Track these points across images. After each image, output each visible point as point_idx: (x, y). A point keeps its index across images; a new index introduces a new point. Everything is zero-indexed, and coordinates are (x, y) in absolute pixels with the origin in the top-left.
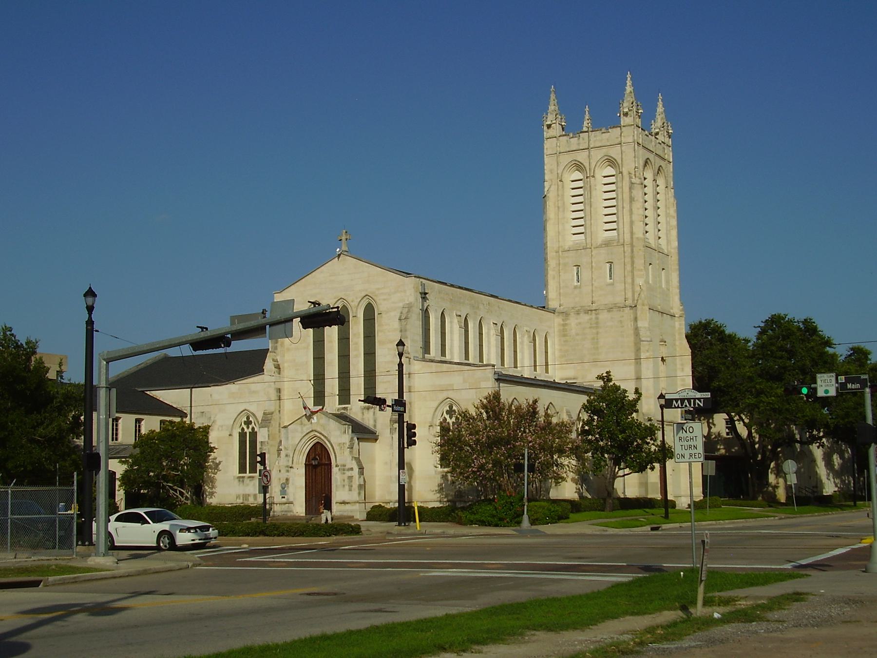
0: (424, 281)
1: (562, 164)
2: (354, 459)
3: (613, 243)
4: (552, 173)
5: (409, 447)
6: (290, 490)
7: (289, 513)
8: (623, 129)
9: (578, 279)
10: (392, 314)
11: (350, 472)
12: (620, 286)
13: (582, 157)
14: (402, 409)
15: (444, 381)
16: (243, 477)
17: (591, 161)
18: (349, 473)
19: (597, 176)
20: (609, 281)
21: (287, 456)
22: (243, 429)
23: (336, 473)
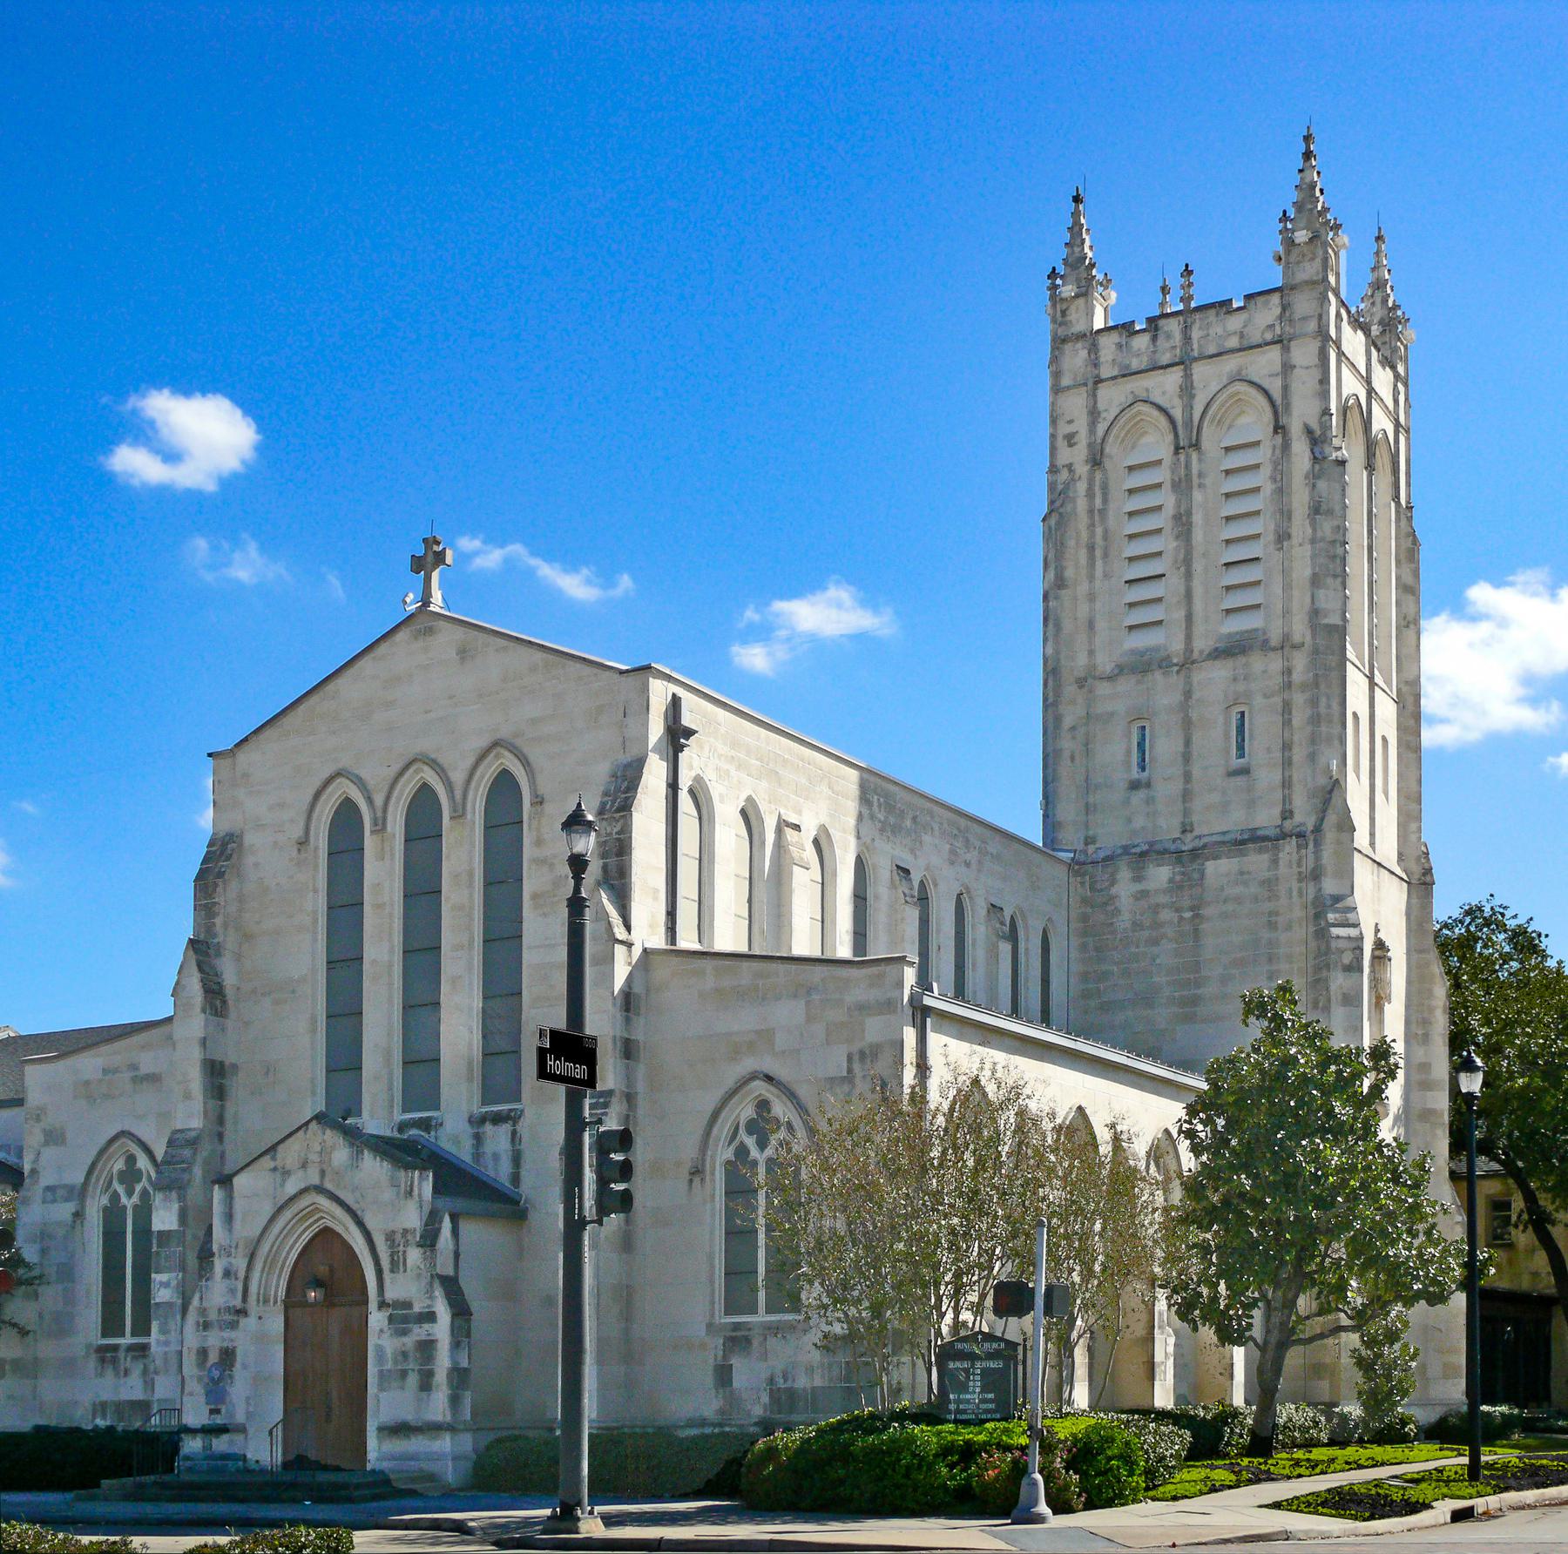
0: (680, 692)
2: (437, 1284)
5: (605, 1219)
6: (239, 1390)
7: (230, 1463)
9: (1144, 760)
11: (426, 1326)
12: (1267, 776)
14: (580, 1071)
16: (115, 1348)
18: (419, 1332)
19: (1206, 443)
20: (1237, 763)
21: (227, 1274)
22: (115, 1197)
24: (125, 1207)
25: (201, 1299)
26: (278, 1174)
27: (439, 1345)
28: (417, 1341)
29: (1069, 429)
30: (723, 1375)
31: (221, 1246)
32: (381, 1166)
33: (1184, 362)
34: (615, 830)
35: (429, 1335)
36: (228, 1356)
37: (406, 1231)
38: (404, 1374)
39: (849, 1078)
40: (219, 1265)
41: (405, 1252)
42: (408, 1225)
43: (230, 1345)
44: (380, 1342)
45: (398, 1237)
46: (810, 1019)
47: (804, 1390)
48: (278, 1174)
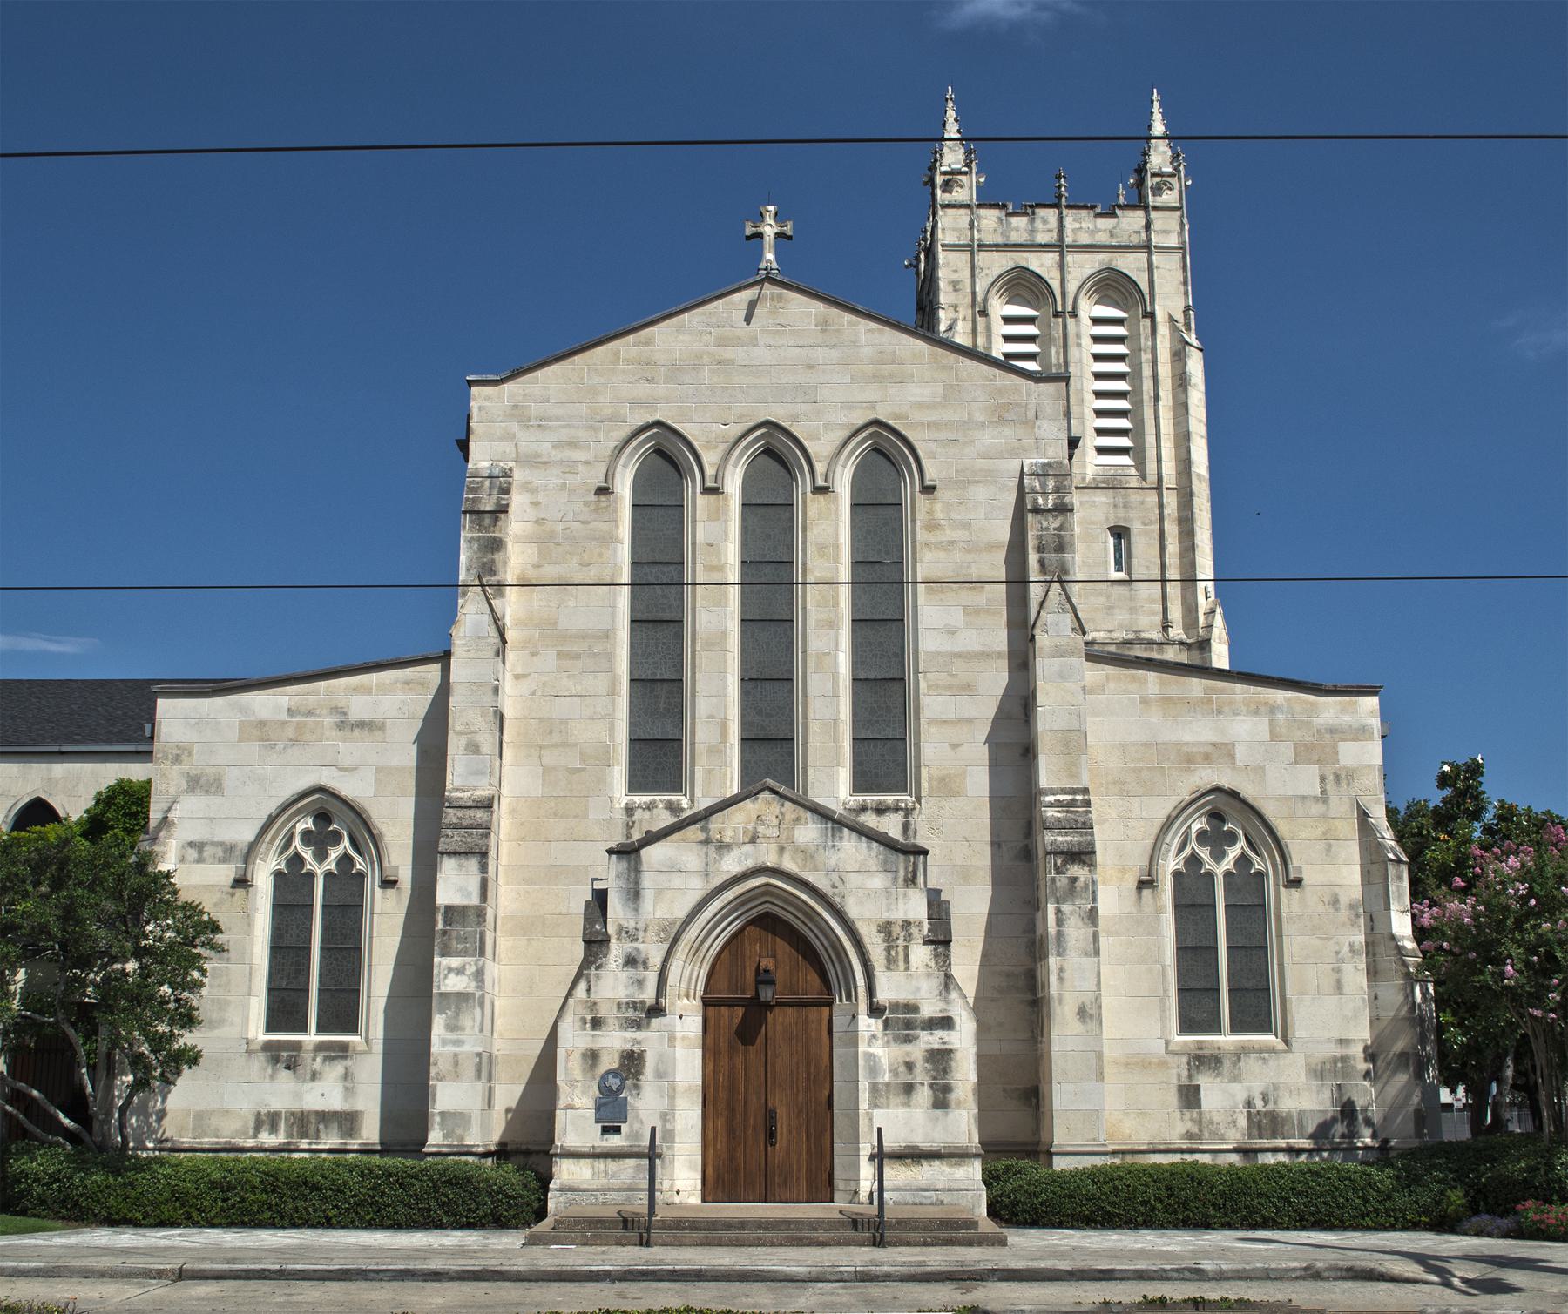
1: (986, 271)
3: (1127, 482)
4: (956, 290)
6: (645, 1105)
8: (1153, 214)
10: (980, 493)
11: (939, 1033)
13: (1042, 264)
15: (1198, 731)
17: (1068, 277)
18: (929, 1040)
21: (631, 961)
23: (874, 1037)
24: (311, 875)
25: (589, 990)
26: (712, 848)
27: (958, 1056)
28: (927, 1051)
29: (955, 277)
30: (1190, 1096)
31: (621, 928)
32: (869, 848)
33: (1059, 247)
34: (1054, 525)
35: (944, 1043)
36: (632, 1062)
37: (907, 924)
38: (909, 1089)
39: (1324, 798)
40: (617, 951)
41: (906, 947)
42: (911, 916)
43: (635, 1049)
44: (871, 1050)
45: (896, 930)
46: (1274, 736)
47: (1289, 1113)
48: (712, 848)
